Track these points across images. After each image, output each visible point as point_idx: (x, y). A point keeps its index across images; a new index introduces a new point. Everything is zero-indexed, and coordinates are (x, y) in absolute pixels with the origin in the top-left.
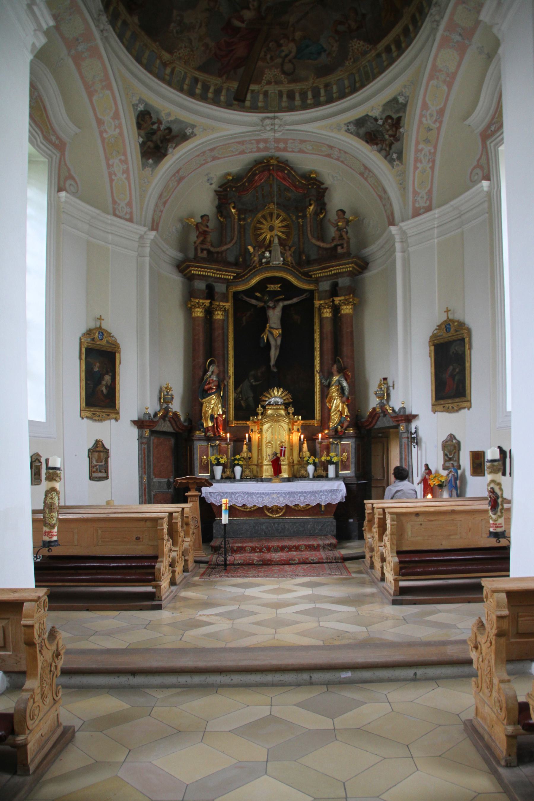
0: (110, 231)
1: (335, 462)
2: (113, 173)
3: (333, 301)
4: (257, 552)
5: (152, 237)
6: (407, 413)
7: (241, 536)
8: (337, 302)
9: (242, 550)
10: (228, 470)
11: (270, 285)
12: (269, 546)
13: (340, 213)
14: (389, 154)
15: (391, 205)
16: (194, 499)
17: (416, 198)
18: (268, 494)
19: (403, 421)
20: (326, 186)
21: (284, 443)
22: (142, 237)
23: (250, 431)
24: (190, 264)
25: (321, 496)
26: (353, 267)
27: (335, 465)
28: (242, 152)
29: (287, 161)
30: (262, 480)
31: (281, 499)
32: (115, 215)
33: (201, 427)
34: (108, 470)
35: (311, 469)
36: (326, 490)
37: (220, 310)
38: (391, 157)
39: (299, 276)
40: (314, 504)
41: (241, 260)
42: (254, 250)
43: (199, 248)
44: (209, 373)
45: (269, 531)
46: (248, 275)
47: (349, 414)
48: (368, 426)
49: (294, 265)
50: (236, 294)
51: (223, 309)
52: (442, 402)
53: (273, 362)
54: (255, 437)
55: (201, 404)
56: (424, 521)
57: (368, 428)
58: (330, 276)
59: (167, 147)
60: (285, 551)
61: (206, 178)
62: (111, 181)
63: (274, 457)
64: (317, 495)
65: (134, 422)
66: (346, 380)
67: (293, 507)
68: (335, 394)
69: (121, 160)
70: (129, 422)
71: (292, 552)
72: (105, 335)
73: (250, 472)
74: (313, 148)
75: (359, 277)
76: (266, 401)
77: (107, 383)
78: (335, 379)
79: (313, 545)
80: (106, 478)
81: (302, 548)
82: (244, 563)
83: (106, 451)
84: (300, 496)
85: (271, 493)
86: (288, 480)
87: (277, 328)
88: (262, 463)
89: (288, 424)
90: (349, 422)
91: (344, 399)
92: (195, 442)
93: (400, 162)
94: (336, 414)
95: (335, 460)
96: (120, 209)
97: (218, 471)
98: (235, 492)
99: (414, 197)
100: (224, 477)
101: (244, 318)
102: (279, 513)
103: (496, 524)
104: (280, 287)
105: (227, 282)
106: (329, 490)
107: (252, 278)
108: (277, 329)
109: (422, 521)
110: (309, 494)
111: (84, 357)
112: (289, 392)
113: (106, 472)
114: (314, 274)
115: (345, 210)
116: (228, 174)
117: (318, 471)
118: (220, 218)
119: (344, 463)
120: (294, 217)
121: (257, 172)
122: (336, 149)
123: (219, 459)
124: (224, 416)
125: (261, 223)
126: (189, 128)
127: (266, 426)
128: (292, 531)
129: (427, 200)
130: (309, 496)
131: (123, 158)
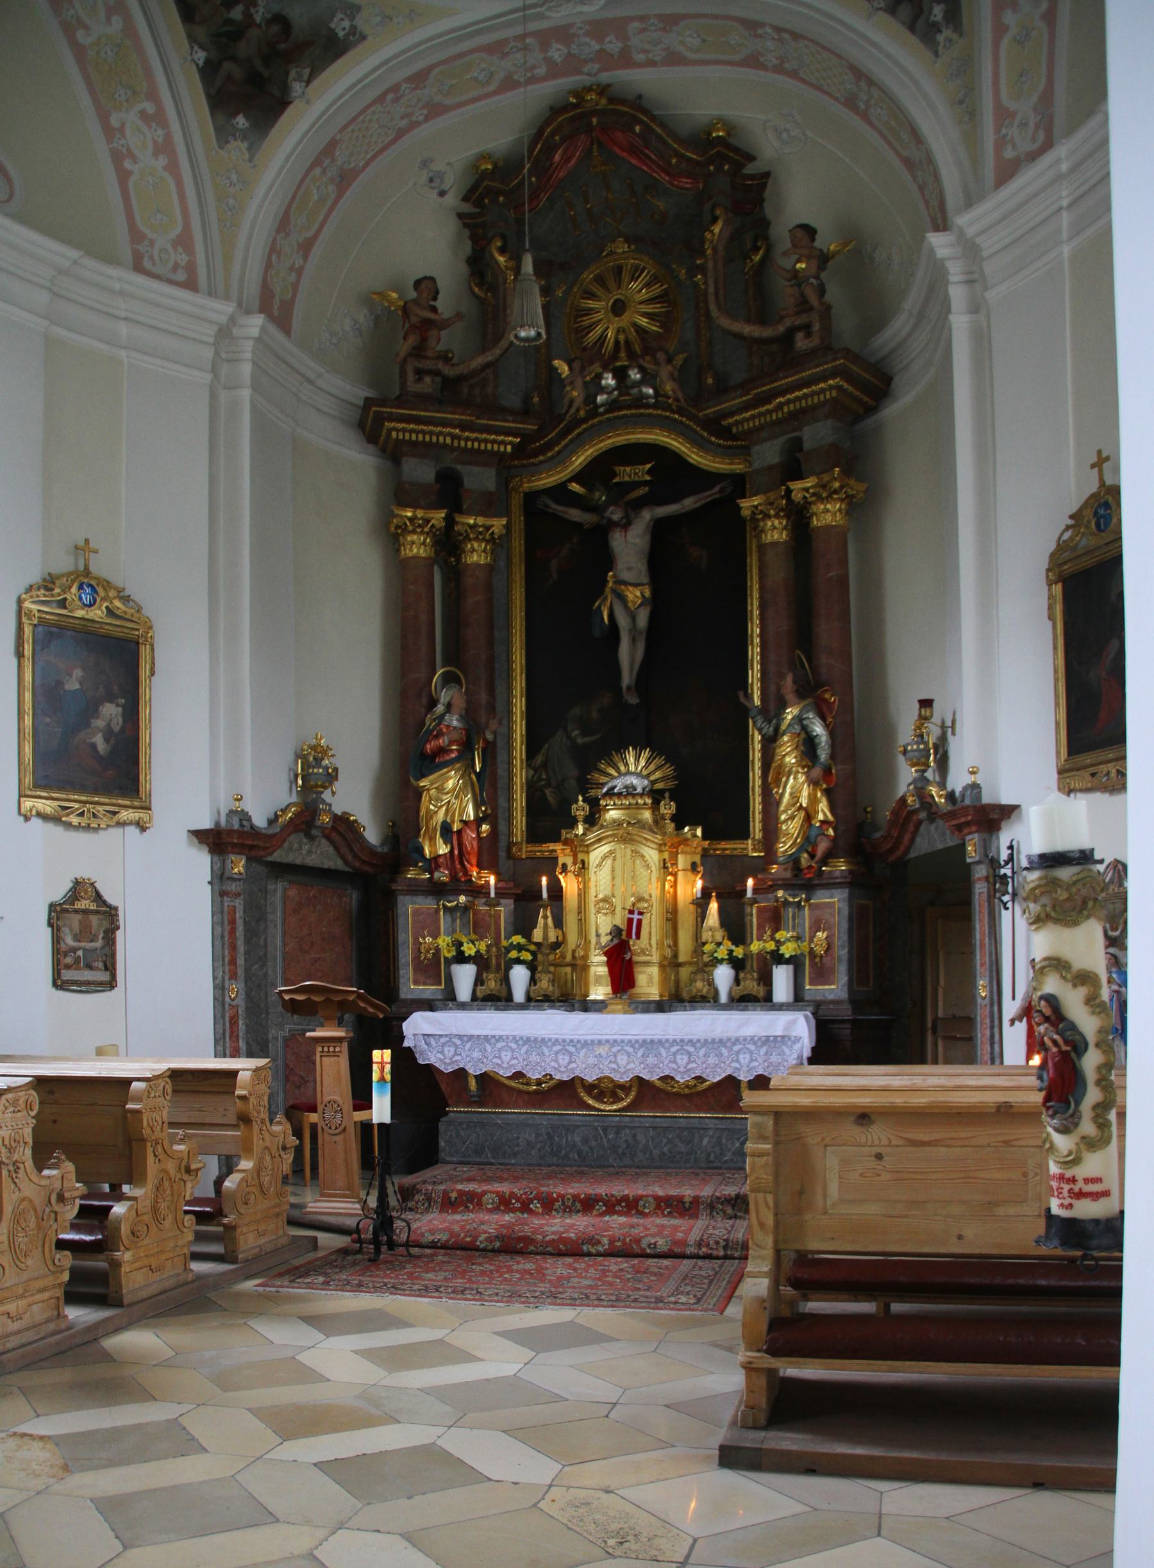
0: (123, 314)
1: (787, 956)
2: (124, 151)
3: (789, 492)
4: (513, 1211)
5: (255, 332)
6: (986, 799)
7: (513, 1161)
8: (797, 496)
9: (472, 1202)
10: (491, 976)
11: (622, 469)
12: (550, 1194)
13: (800, 234)
14: (921, 12)
15: (937, 177)
16: (332, 1049)
17: (1004, 131)
18: (585, 1044)
19: (974, 828)
20: (766, 169)
21: (647, 901)
22: (224, 333)
23: (559, 870)
24: (382, 412)
25: (738, 1053)
26: (839, 388)
27: (791, 968)
28: (509, 84)
29: (640, 97)
30: (586, 1006)
31: (506, 1056)
32: (138, 268)
33: (415, 856)
34: (114, 964)
35: (723, 976)
36: (752, 1038)
37: (476, 539)
38: (928, 19)
39: (702, 436)
40: (718, 1078)
41: (536, 400)
42: (571, 369)
43: (410, 370)
44: (440, 708)
45: (591, 1148)
46: (563, 443)
47: (830, 818)
48: (891, 851)
49: (683, 404)
50: (531, 497)
51: (488, 537)
52: (1087, 758)
53: (627, 679)
54: (569, 884)
55: (418, 793)
56: (889, 1145)
57: (892, 858)
58: (778, 422)
59: (287, 78)
60: (595, 1212)
61: (424, 176)
62: (123, 177)
63: (612, 940)
64: (725, 1052)
65: (200, 836)
66: (823, 718)
67: (659, 1084)
68: (791, 760)
69: (143, 114)
70: (185, 835)
71: (615, 1217)
72: (101, 592)
73: (553, 981)
74: (704, 41)
75: (870, 422)
76: (603, 785)
77: (109, 725)
78: (789, 717)
79: (680, 1200)
80: (111, 984)
81: (645, 1207)
82: (447, 1241)
83: (110, 914)
84: (675, 1054)
85: (593, 1041)
86: (660, 1007)
87: (637, 582)
88: (586, 957)
89: (660, 848)
90: (834, 840)
91: (817, 772)
92: (400, 898)
93: (954, 31)
94: (792, 818)
95: (787, 950)
96: (156, 254)
97: (464, 977)
98: (494, 1036)
99: (998, 131)
100: (479, 994)
101: (554, 565)
102: (622, 1099)
103: (1073, 1180)
104: (649, 472)
105: (501, 462)
106: (760, 1039)
107: (574, 452)
108: (636, 585)
109: (885, 1142)
110: (702, 1046)
111: (28, 650)
112: (667, 761)
113: (106, 969)
114: (737, 423)
115: (813, 224)
116: (484, 157)
117: (742, 984)
118: (476, 290)
119: (817, 960)
120: (684, 271)
121: (557, 138)
122: (768, 30)
123: (461, 944)
124: (485, 827)
125: (592, 296)
126: (340, 16)
127: (595, 856)
128: (656, 1152)
129: (1037, 127)
130: (702, 1052)
131: (150, 108)
